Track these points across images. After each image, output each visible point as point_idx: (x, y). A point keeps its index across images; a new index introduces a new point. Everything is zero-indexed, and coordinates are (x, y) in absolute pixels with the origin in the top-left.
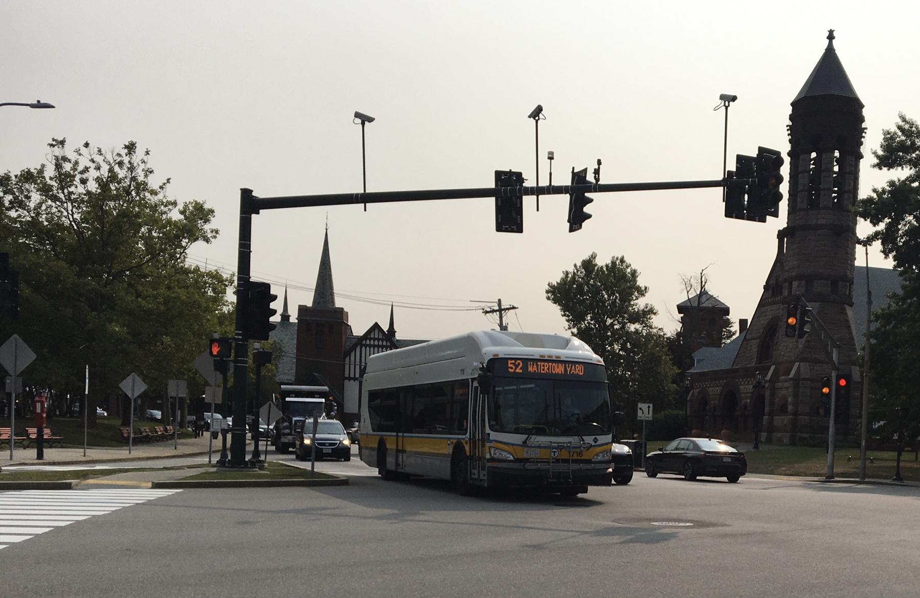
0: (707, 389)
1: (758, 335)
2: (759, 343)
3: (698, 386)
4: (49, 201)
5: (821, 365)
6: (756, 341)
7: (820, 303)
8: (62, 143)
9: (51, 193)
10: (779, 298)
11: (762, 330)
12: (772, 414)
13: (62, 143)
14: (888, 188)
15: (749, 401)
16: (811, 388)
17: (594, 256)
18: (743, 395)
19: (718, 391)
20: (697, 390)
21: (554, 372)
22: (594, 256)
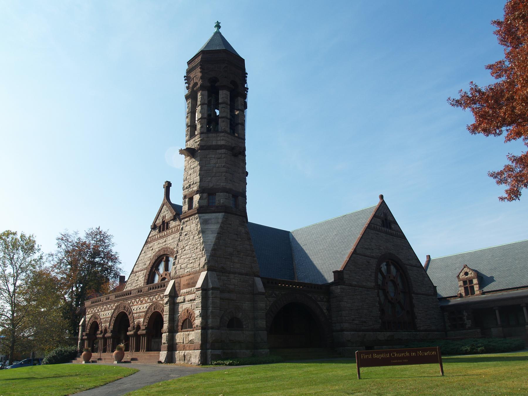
0: (99, 314)
1: (145, 266)
2: (146, 273)
3: (90, 312)
4: (59, 278)
5: (227, 274)
6: (142, 272)
7: (223, 214)
8: (461, 90)
9: (110, 264)
10: (166, 233)
11: (149, 262)
12: (173, 331)
13: (461, 90)
14: (18, 237)
15: (142, 320)
16: (221, 299)
17: (474, 129)
18: (135, 315)
19: (110, 314)
20: (89, 316)
21: (399, 356)
22: (474, 129)
